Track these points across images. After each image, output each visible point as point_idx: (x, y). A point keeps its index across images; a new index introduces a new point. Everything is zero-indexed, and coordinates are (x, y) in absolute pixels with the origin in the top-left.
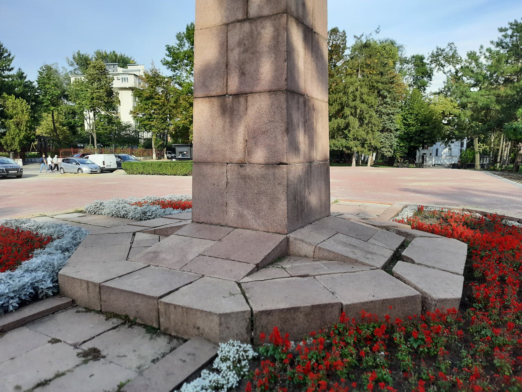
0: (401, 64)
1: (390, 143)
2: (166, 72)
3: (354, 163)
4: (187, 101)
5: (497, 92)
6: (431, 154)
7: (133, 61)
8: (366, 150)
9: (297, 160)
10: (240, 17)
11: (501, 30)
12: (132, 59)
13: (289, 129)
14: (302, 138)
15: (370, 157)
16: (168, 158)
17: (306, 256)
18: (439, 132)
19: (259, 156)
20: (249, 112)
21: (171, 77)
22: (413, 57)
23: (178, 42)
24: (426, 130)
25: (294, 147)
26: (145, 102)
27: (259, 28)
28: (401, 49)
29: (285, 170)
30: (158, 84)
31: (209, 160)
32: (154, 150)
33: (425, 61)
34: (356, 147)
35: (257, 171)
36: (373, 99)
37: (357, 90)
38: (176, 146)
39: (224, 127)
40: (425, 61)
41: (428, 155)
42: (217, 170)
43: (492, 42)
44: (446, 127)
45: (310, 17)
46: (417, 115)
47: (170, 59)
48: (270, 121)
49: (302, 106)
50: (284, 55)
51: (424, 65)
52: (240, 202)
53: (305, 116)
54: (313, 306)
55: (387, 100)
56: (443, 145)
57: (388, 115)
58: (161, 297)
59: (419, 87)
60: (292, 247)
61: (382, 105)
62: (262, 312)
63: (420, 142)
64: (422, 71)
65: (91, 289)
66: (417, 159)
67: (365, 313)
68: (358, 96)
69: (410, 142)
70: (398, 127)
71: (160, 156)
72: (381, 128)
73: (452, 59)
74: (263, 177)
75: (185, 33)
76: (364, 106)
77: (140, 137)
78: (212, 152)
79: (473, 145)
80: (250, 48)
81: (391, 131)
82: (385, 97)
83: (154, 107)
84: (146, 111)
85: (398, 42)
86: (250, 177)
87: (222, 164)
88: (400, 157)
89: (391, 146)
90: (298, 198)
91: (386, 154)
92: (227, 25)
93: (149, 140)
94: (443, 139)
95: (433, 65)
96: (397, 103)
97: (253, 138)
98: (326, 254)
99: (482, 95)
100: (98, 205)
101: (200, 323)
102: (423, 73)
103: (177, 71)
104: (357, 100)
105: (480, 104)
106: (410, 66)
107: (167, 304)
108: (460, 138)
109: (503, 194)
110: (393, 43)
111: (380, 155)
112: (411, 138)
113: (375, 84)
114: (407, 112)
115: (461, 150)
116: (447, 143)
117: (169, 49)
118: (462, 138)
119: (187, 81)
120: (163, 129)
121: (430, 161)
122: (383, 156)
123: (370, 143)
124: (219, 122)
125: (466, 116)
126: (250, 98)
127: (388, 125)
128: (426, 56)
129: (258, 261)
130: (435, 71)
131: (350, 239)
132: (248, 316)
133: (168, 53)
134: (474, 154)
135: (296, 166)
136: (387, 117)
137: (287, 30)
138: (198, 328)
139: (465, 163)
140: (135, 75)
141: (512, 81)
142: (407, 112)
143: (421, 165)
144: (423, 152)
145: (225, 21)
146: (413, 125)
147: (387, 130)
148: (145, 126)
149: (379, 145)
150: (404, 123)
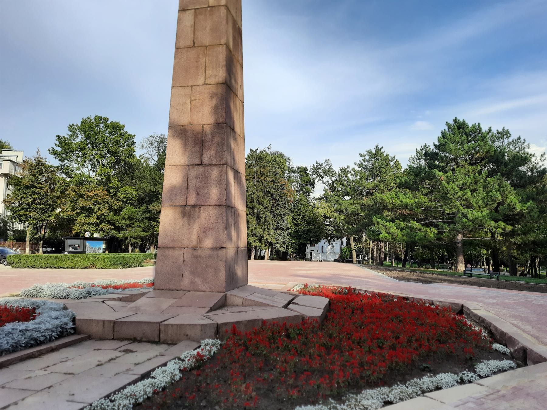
0: (289, 173)
1: (283, 241)
2: (53, 161)
3: (253, 257)
4: (76, 192)
5: (362, 202)
6: (317, 251)
7: (8, 145)
8: (263, 246)
9: (231, 246)
10: (197, 162)
11: (361, 155)
12: (6, 144)
13: (227, 227)
14: (234, 233)
15: (267, 251)
16: (44, 252)
17: (237, 305)
18: (322, 232)
19: (208, 243)
20: (201, 216)
21: (58, 167)
22: (298, 168)
23: (70, 133)
24: (312, 229)
25: (230, 238)
26: (24, 191)
27: (209, 171)
28: (288, 161)
29: (224, 252)
30: (42, 173)
31: (170, 246)
32: (28, 243)
33: (308, 172)
34: (255, 242)
35: (207, 252)
36: (267, 201)
37: (254, 194)
38: (66, 239)
39: (183, 225)
40: (308, 172)
41: (315, 251)
42: (176, 253)
43: (355, 164)
44: (328, 227)
45: (237, 164)
46: (304, 216)
47: (59, 149)
48: (215, 223)
49: (233, 214)
50: (224, 187)
51: (307, 175)
52: (193, 273)
53: (234, 220)
54: (249, 321)
55: (279, 203)
56: (327, 243)
57: (280, 215)
58: (161, 322)
59: (304, 193)
60: (228, 301)
61: (275, 207)
62: (223, 324)
63: (308, 240)
64: (306, 181)
65: (106, 326)
66: (307, 255)
67: (275, 322)
68: (255, 199)
69: (300, 239)
70: (289, 226)
71: (34, 250)
72: (275, 227)
73: (329, 172)
74: (210, 256)
75: (79, 125)
76: (260, 207)
77: (8, 228)
78: (174, 241)
79: (350, 244)
80: (204, 180)
81: (283, 230)
82: (277, 201)
83: (35, 197)
84: (24, 200)
85: (286, 155)
86: (200, 257)
87: (180, 248)
88: (292, 252)
89: (284, 243)
90: (231, 270)
91: (280, 249)
92: (188, 166)
93: (23, 232)
94: (327, 237)
95: (315, 176)
96: (287, 206)
97: (205, 231)
98: (250, 302)
99: (351, 204)
100: (37, 289)
101: (188, 332)
102: (307, 182)
103: (66, 161)
104: (255, 202)
105: (350, 210)
106: (296, 175)
107: (167, 325)
108: (340, 238)
109: (361, 278)
110: (281, 155)
111: (274, 252)
112: (301, 236)
113: (269, 189)
114: (295, 213)
115: (341, 248)
116: (330, 241)
117: (59, 139)
118: (341, 238)
119: (78, 172)
120: (42, 221)
121: (317, 257)
122: (277, 252)
123: (266, 239)
124: (180, 222)
125: (340, 219)
126: (202, 208)
127: (281, 224)
128: (309, 168)
129: (211, 306)
130: (317, 180)
131: (262, 296)
132: (216, 326)
133: (57, 143)
134: (352, 251)
135: (231, 250)
136: (280, 218)
137: (226, 173)
138: (187, 335)
139: (345, 258)
140: (11, 161)
141: (372, 194)
142: (295, 213)
143: (311, 260)
144: (311, 248)
145: (187, 163)
146: (301, 225)
147: (280, 228)
148: (21, 216)
149: (274, 241)
150: (294, 223)
